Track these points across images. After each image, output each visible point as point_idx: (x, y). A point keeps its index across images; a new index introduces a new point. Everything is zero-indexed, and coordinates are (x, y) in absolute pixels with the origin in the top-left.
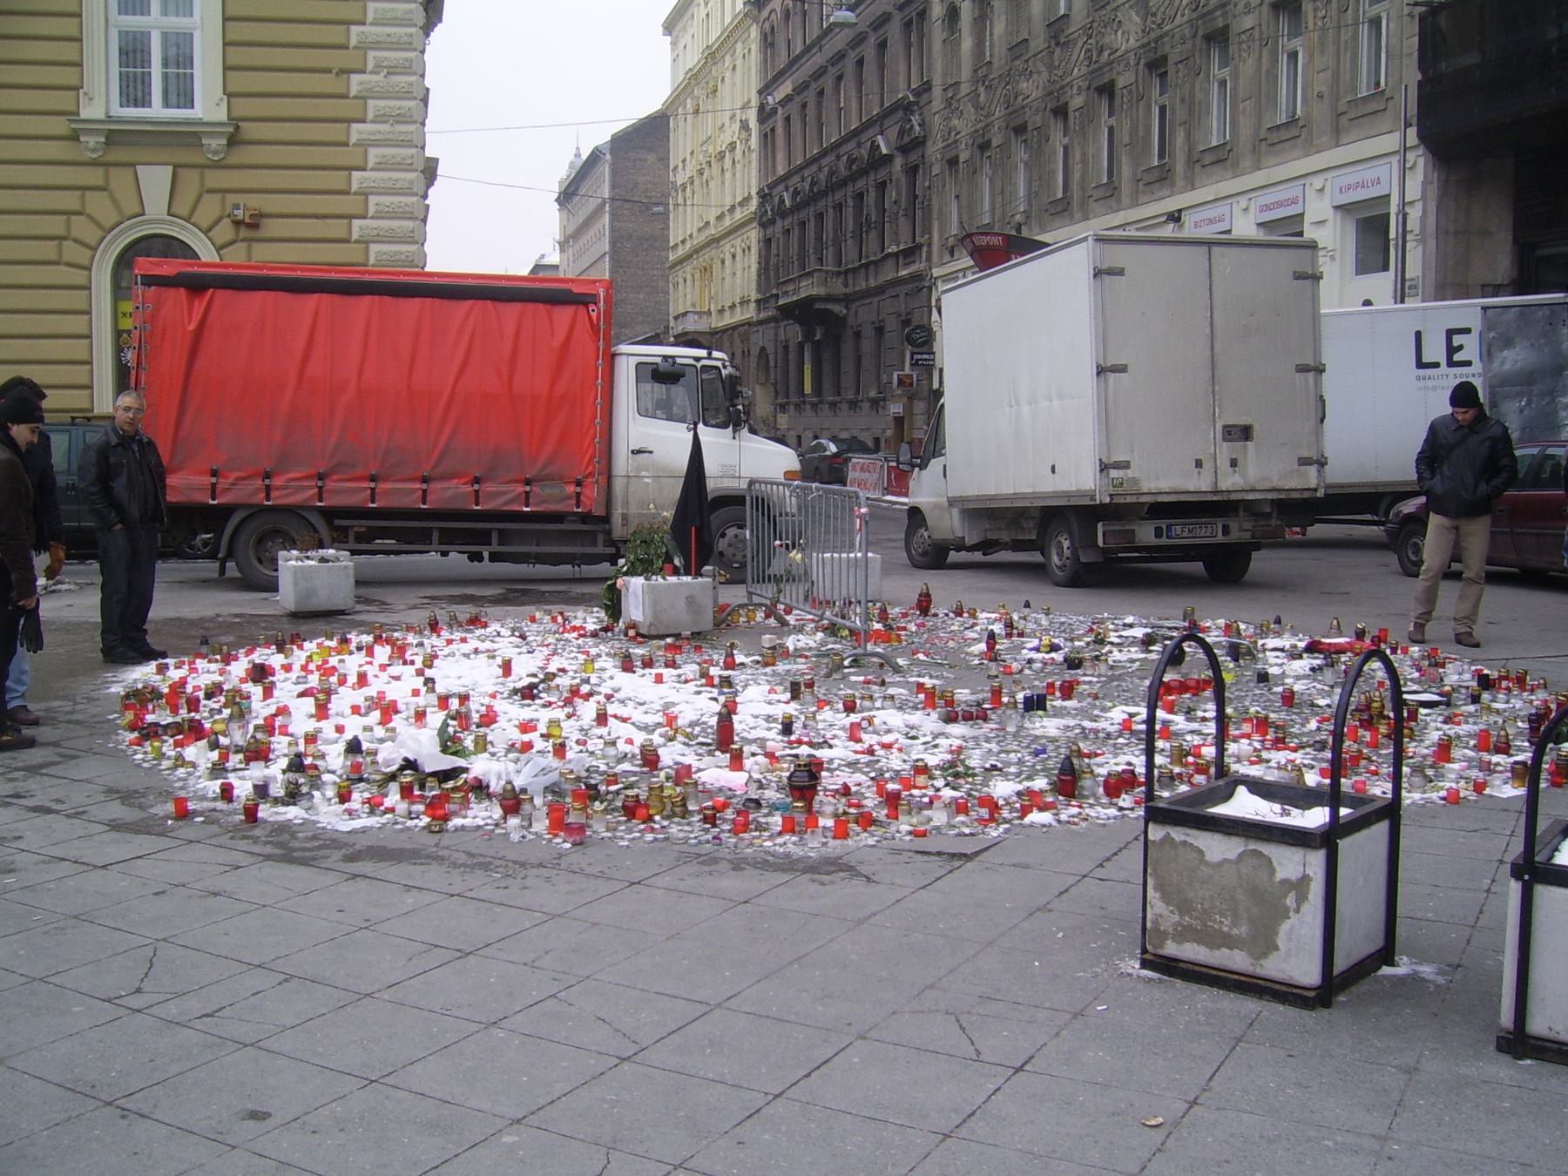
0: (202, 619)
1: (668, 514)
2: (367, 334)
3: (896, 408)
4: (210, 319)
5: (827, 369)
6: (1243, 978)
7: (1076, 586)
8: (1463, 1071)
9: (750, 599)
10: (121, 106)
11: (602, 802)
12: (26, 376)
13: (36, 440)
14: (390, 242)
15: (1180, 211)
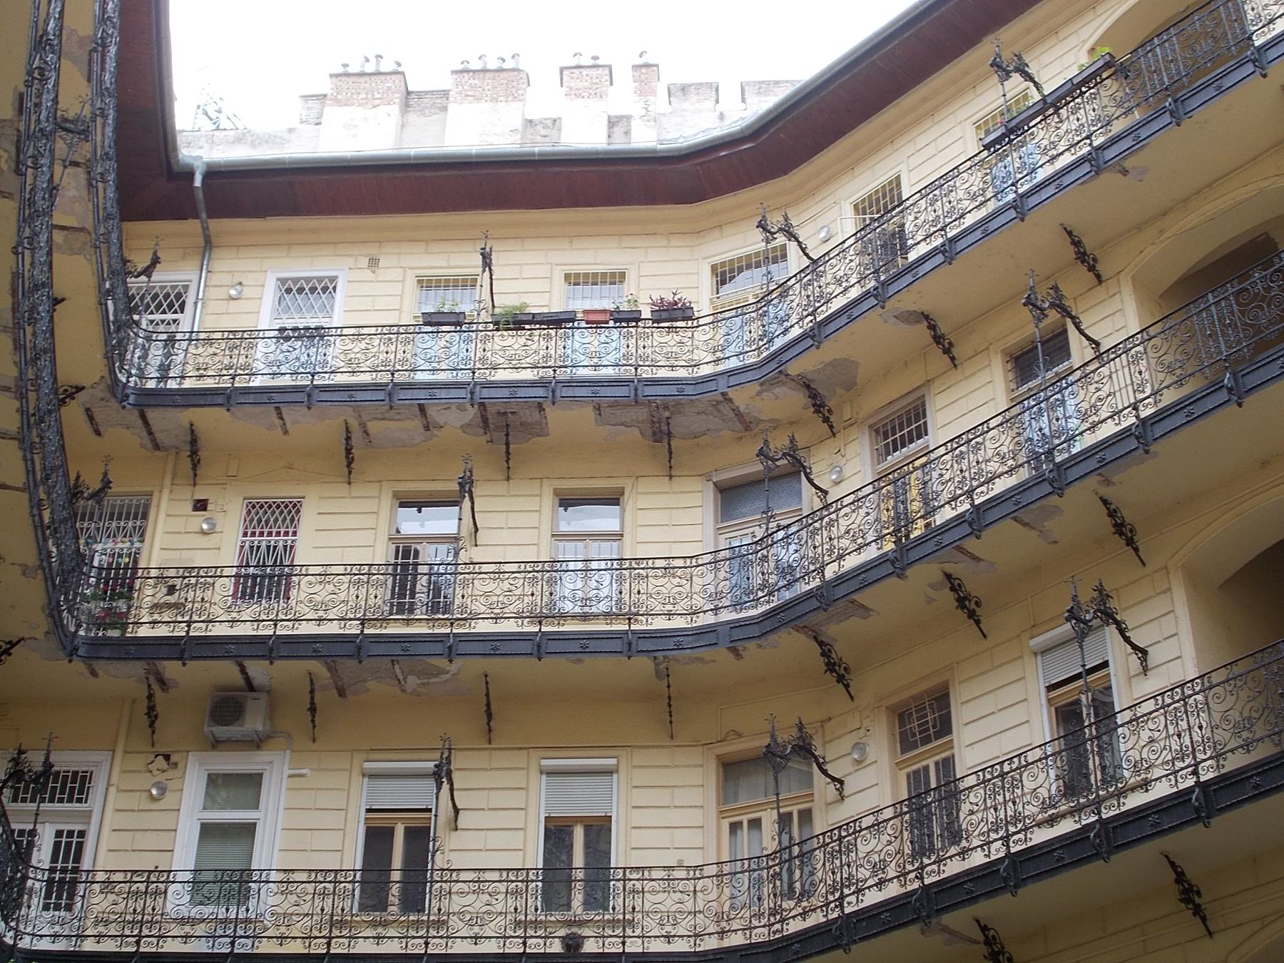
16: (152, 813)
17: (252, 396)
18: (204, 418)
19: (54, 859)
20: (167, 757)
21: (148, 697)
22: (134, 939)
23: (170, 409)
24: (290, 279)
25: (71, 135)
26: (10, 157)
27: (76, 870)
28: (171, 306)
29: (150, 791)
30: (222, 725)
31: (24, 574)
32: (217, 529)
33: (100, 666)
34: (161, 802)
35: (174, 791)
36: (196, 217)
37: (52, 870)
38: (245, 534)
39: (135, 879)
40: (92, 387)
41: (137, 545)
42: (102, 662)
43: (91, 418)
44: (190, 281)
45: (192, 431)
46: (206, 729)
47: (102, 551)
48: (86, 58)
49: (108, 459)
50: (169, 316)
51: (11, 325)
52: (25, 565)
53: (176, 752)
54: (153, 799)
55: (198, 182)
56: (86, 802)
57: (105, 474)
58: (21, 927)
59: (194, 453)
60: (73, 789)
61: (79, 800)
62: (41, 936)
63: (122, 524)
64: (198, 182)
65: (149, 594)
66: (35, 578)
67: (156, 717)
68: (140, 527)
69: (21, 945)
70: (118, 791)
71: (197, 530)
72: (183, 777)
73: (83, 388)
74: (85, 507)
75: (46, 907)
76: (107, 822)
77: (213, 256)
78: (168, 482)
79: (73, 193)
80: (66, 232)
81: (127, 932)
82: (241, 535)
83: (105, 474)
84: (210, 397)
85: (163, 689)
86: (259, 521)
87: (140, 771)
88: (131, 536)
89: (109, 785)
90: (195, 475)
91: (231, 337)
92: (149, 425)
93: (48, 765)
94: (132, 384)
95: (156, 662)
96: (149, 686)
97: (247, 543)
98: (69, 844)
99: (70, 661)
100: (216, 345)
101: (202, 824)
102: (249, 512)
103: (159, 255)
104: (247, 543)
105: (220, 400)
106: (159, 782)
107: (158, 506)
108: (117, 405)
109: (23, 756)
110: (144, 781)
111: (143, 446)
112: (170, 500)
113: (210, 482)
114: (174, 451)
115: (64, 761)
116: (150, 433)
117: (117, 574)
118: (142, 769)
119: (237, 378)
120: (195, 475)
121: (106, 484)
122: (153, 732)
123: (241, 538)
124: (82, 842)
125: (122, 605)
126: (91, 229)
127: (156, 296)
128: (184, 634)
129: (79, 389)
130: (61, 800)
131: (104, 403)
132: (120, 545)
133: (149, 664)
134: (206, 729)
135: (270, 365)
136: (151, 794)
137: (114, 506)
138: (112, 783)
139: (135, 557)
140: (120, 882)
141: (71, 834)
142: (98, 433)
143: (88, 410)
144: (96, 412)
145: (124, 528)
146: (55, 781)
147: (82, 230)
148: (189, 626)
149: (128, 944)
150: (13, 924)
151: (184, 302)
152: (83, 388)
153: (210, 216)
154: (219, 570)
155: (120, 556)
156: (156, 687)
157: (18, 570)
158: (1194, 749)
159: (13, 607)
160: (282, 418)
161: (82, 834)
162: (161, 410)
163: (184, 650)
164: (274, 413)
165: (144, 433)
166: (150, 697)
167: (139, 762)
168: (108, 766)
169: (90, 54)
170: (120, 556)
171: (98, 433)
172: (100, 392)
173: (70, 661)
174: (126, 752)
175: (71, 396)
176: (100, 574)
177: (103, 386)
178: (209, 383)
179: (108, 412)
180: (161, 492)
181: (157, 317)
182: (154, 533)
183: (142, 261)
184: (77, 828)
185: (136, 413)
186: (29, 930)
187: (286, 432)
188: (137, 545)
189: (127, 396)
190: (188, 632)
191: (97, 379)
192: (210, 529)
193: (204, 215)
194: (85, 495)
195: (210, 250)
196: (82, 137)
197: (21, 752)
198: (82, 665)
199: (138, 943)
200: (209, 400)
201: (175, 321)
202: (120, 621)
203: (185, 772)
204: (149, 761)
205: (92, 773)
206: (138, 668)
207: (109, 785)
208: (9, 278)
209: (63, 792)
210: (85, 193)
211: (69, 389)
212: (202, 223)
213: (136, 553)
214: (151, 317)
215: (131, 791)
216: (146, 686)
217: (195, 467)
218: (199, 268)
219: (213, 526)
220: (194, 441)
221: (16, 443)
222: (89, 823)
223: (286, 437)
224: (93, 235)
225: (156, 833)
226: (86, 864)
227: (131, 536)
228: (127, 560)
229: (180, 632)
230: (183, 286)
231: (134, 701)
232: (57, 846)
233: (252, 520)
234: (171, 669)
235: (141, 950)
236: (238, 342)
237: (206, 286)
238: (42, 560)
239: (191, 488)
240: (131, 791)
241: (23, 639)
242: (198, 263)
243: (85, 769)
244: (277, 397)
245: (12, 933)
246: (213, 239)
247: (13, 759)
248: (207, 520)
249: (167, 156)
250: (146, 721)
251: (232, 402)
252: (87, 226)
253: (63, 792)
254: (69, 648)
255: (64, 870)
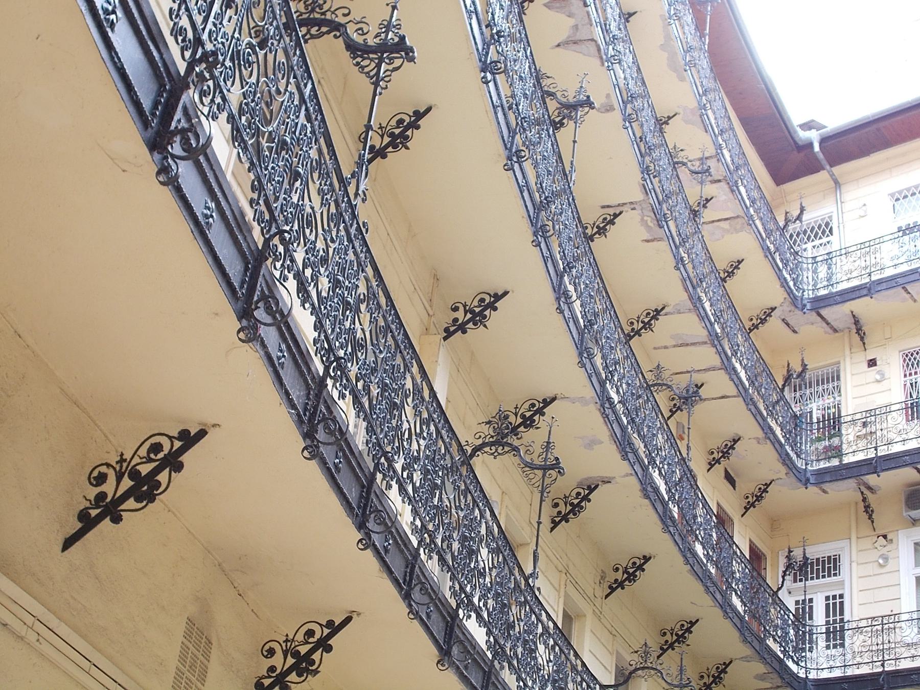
0: (135, 92)
1: (314, 461)
2: (554, 554)
3: (257, 107)
4: (283, 661)
5: (161, 46)
6: (754, 66)
7: (740, 121)
8: (312, 111)
9: (311, 34)
10: (615, 109)
11: (267, 220)
12: (139, 504)
13: (169, 148)
14: (595, 7)
15: (859, 218)
16: (882, 576)
17: (884, 284)
18: (859, 306)
19: (827, 616)
20: (885, 537)
21: (863, 501)
22: (880, 663)
23: (835, 306)
24: (897, 192)
25: (700, 175)
26: (652, 218)
27: (842, 620)
28: (824, 232)
29: (878, 561)
30: (914, 510)
31: (759, 443)
32: (887, 376)
33: (826, 486)
34: (888, 566)
35: (895, 558)
36: (823, 169)
37: (828, 623)
38: (905, 376)
39: (874, 623)
40: (781, 305)
41: (838, 398)
42: (827, 484)
43: (788, 324)
44: (832, 212)
45: (854, 316)
46: (905, 514)
47: (816, 408)
48: (699, 119)
49: (802, 350)
50: (824, 240)
51: (692, 307)
52: (758, 438)
53: (891, 532)
54: (881, 566)
55: (817, 148)
56: (839, 575)
57: (803, 360)
58: (809, 666)
59: (858, 330)
60: (829, 568)
61: (835, 575)
62: (822, 669)
63: (826, 386)
64: (817, 148)
65: (849, 433)
66: (766, 444)
67: (872, 511)
68: (837, 386)
69: (811, 676)
70: (858, 564)
71: (874, 380)
72: (897, 548)
73: (776, 308)
74: (796, 382)
75: (828, 647)
76: (854, 586)
77: (843, 191)
78: (847, 352)
79: (724, 197)
80: (729, 221)
81: (875, 659)
82: (903, 376)
83: (803, 360)
84: (857, 292)
85: (872, 493)
86: (913, 365)
87: (870, 549)
88: (833, 393)
89: (851, 562)
90: (864, 344)
91: (863, 247)
92: (825, 319)
93: (806, 558)
94: (806, 296)
95: (861, 477)
96: (862, 493)
97: (908, 381)
98: (834, 604)
99: (806, 488)
100: (854, 255)
101: (916, 577)
102: (905, 360)
103: (803, 205)
104: (908, 381)
105: (865, 292)
106: (883, 554)
107: (845, 370)
108: (800, 312)
109: (792, 554)
110: (874, 555)
111: (826, 333)
112: (852, 364)
113: (874, 346)
114: (847, 330)
115: (816, 552)
116: (828, 324)
117: (824, 424)
118: (870, 546)
119: (872, 274)
120: (864, 344)
121: (804, 367)
122: (873, 522)
123: (903, 379)
124: (843, 602)
125: (836, 441)
126: (743, 215)
127: (813, 228)
128: (874, 456)
129: (773, 309)
130: (824, 577)
131: (791, 313)
132: (827, 401)
133: (857, 480)
134: (905, 514)
135: (892, 259)
136: (879, 563)
137: (818, 376)
138: (852, 560)
139: (838, 407)
140: (865, 627)
141: (834, 597)
142: (795, 331)
143: (783, 320)
144: (788, 320)
145: (827, 389)
146: (818, 565)
147: (738, 217)
148: (876, 450)
149: (877, 667)
150: (803, 664)
151: (831, 228)
152: (776, 308)
153: (831, 166)
154: (888, 407)
155: (829, 408)
156: (866, 492)
157: (755, 441)
158: (883, 631)
159: (760, 463)
160: (909, 293)
161: (841, 596)
162: (829, 308)
163: (876, 467)
164: (903, 291)
165: (824, 325)
166: (864, 500)
167: (867, 543)
168: (849, 547)
169: (701, 117)
170: (829, 408)
171: (795, 331)
172: (787, 307)
173: (806, 488)
174: (858, 538)
175: (769, 315)
176: (819, 425)
177: (787, 303)
178: (855, 283)
179: (796, 318)
180: (844, 360)
181: (817, 242)
182: (846, 389)
183: (796, 213)
184: (837, 593)
185: (814, 314)
186: (814, 666)
187: (915, 301)
188: (838, 398)
189: (805, 306)
190: (876, 454)
191: (782, 300)
192: (881, 378)
193: (828, 167)
194: (795, 376)
195: (840, 187)
196: (707, 174)
197: (790, 552)
198: (815, 488)
199: (883, 665)
200: (857, 294)
201: (828, 242)
202: (838, 452)
203: (898, 545)
204: (874, 541)
205: (839, 555)
206: (852, 483)
207: (851, 562)
208: (680, 282)
209: (823, 571)
210: (730, 195)
211: (767, 311)
212: (828, 172)
213: (838, 404)
214: (814, 244)
215: (866, 563)
216: (860, 493)
217: (862, 339)
218: (836, 202)
219: (883, 375)
220: (857, 322)
221: (723, 371)
222: (844, 589)
223: (916, 304)
224: (746, 218)
225: (887, 588)
226: (847, 617)
227: (833, 393)
228: (834, 410)
229: (871, 454)
230: (829, 217)
231: (856, 503)
232: (827, 606)
233: (908, 365)
234: (872, 479)
235: (886, 669)
236: (868, 249)
237: (842, 213)
238: (766, 433)
239: (863, 353)
240: (866, 563)
241: (773, 480)
242: (833, 199)
243: (835, 554)
244: (901, 281)
245: (803, 670)
246: (839, 180)
247: (787, 557)
248: (878, 372)
249: (792, 138)
250: (866, 516)
251: (872, 291)
252: (740, 214)
253: (823, 571)
254: (804, 480)
255: (835, 622)
